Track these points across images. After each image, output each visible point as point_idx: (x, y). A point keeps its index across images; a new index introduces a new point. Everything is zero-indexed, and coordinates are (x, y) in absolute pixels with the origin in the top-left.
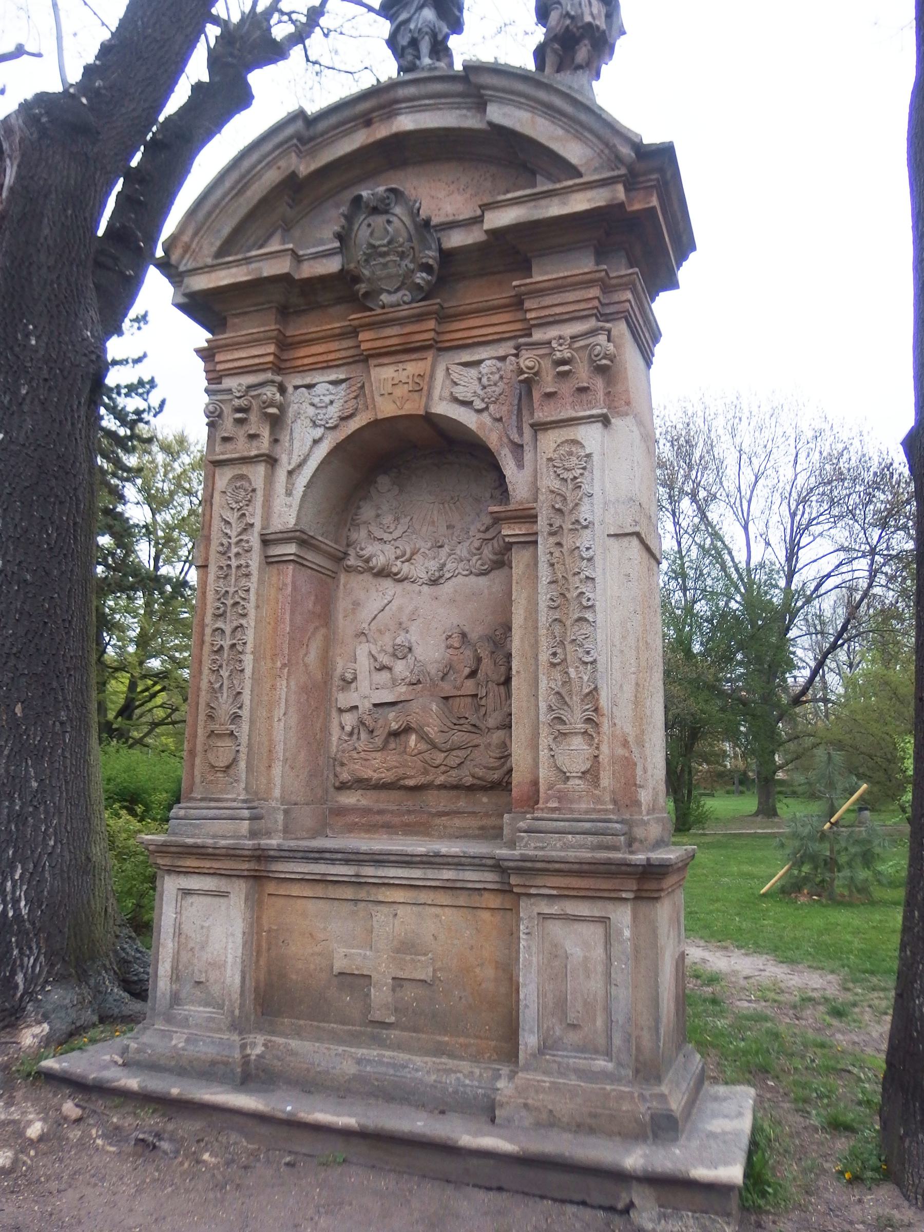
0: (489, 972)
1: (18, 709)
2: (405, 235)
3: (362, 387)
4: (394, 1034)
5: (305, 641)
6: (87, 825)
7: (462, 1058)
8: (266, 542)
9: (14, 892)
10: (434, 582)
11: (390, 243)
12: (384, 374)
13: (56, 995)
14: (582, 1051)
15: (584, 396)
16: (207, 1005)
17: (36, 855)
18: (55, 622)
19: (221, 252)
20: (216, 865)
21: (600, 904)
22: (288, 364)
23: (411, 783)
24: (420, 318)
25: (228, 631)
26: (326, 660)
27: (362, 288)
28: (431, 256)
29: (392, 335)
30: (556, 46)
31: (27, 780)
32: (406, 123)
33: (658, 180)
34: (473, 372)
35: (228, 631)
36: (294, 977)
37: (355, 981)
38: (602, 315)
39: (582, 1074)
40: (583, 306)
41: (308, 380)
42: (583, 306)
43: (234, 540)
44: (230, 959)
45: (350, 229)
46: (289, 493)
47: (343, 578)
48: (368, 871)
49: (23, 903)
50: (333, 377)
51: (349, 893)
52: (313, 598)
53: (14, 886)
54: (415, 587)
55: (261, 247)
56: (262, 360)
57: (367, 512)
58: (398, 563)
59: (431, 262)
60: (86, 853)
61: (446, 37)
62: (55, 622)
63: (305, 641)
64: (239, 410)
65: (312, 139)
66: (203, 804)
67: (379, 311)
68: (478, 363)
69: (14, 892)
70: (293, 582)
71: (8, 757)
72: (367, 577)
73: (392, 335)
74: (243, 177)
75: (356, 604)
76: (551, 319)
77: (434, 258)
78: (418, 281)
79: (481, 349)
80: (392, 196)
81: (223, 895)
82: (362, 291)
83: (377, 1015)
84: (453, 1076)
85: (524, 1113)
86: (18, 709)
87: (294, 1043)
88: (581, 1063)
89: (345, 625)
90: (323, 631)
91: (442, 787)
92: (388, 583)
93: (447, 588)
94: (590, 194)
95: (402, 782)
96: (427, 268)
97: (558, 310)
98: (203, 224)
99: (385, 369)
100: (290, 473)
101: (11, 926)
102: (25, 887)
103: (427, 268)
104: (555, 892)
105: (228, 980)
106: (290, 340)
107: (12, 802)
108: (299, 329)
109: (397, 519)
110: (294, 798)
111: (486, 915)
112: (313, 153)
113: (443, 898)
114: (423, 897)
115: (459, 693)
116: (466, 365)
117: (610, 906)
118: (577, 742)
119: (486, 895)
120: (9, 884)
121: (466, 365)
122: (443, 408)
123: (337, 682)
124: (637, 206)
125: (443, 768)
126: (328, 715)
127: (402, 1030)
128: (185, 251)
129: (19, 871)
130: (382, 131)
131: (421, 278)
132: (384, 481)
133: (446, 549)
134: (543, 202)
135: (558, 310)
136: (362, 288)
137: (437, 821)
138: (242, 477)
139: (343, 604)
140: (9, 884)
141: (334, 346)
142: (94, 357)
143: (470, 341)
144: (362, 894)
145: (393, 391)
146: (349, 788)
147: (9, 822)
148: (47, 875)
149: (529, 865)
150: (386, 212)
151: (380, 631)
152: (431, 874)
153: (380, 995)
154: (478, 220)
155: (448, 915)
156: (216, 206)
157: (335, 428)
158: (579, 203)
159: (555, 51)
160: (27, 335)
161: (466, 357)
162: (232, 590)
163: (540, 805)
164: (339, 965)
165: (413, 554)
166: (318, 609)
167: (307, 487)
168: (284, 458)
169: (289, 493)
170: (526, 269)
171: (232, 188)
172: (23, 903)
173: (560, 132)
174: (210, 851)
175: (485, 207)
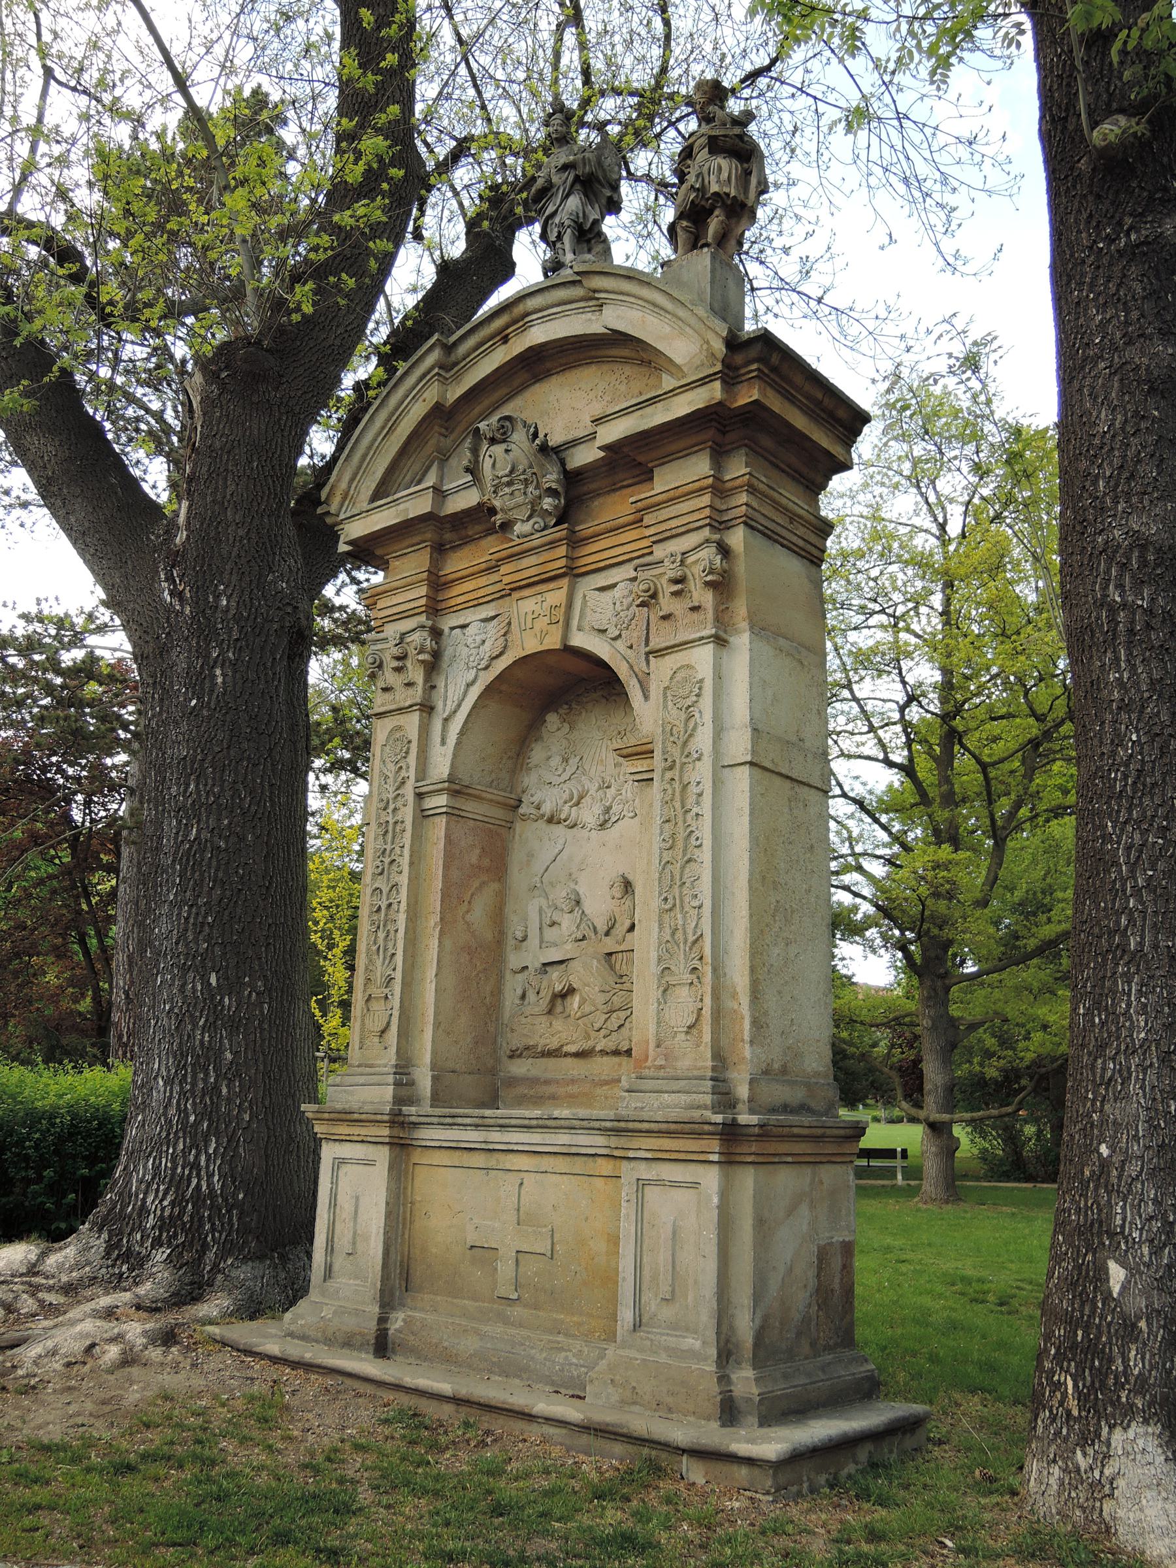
0: (600, 1246)
1: (213, 980)
2: (526, 462)
3: (509, 624)
4: (517, 1311)
5: (467, 898)
6: (290, 1102)
7: (574, 1336)
8: (420, 796)
9: (207, 1167)
10: (602, 826)
11: (511, 472)
12: (528, 605)
13: (244, 1272)
14: (674, 1329)
15: (695, 615)
16: (356, 1278)
17: (231, 1130)
18: (250, 889)
19: (373, 499)
20: (363, 1131)
21: (692, 1167)
22: (443, 605)
23: (572, 1049)
24: (553, 545)
25: (385, 890)
26: (498, 917)
27: (498, 519)
28: (552, 478)
29: (530, 566)
30: (685, 223)
31: (221, 1051)
32: (539, 334)
33: (758, 369)
34: (607, 596)
35: (385, 890)
36: (434, 1250)
37: (483, 1254)
38: (721, 523)
39: (673, 1352)
40: (697, 516)
41: (461, 622)
42: (697, 516)
43: (391, 796)
44: (374, 1231)
45: (477, 461)
46: (443, 743)
47: (518, 826)
48: (495, 1136)
49: (216, 1178)
50: (483, 616)
51: (478, 1160)
52: (478, 851)
53: (208, 1161)
54: (585, 833)
55: (419, 483)
56: (415, 604)
57: (537, 754)
58: (566, 808)
59: (554, 485)
60: (288, 1131)
61: (597, 223)
62: (250, 889)
63: (467, 898)
64: (676, 581)
65: (456, 364)
66: (360, 1070)
67: (518, 541)
68: (614, 586)
69: (207, 1167)
70: (447, 836)
71: (204, 1027)
72: (541, 824)
73: (530, 566)
74: (393, 414)
75: (531, 855)
76: (668, 534)
77: (558, 481)
78: (545, 507)
79: (614, 571)
80: (508, 424)
81: (369, 1163)
82: (498, 523)
83: (502, 1291)
84: (563, 1354)
85: (611, 1390)
86: (213, 980)
87: (430, 1318)
88: (672, 1341)
89: (518, 878)
90: (495, 886)
91: (603, 1053)
92: (559, 830)
93: (613, 833)
94: (690, 396)
95: (565, 1049)
96: (552, 492)
97: (673, 523)
98: (359, 467)
99: (526, 602)
100: (446, 720)
101: (204, 1200)
102: (218, 1162)
103: (552, 492)
104: (649, 1155)
105: (371, 1252)
106: (443, 580)
107: (207, 1074)
108: (457, 563)
109: (566, 760)
110: (451, 1065)
111: (599, 1183)
112: (457, 378)
113: (561, 1164)
114: (546, 1163)
115: (622, 948)
116: (602, 589)
117: (700, 1168)
118: (684, 992)
119: (600, 1160)
120: (203, 1158)
121: (602, 589)
122: (579, 640)
123: (511, 942)
124: (742, 401)
125: (603, 1032)
126: (501, 978)
127: (525, 1306)
128: (344, 499)
129: (213, 1145)
130: (518, 345)
131: (548, 503)
132: (552, 719)
133: (612, 791)
134: (649, 410)
135: (673, 523)
136: (498, 519)
137: (599, 1091)
138: (399, 728)
139: (517, 857)
140: (203, 1158)
141: (482, 581)
142: (289, 610)
143: (602, 564)
144: (492, 1161)
145: (533, 624)
146: (520, 1056)
147: (203, 1095)
148: (241, 1150)
149: (623, 1125)
150: (504, 441)
151: (551, 884)
152: (535, 1138)
153: (505, 1269)
154: (592, 436)
155: (566, 1182)
156: (369, 448)
157: (486, 668)
158: (681, 407)
159: (684, 229)
160: (217, 597)
161: (601, 580)
162: (388, 847)
163: (649, 1063)
164: (472, 1238)
165: (581, 797)
166: (486, 862)
167: (462, 733)
168: (440, 705)
169: (443, 743)
170: (647, 476)
171: (383, 428)
172: (216, 1178)
173: (668, 329)
174: (356, 1116)
175: (597, 421)
